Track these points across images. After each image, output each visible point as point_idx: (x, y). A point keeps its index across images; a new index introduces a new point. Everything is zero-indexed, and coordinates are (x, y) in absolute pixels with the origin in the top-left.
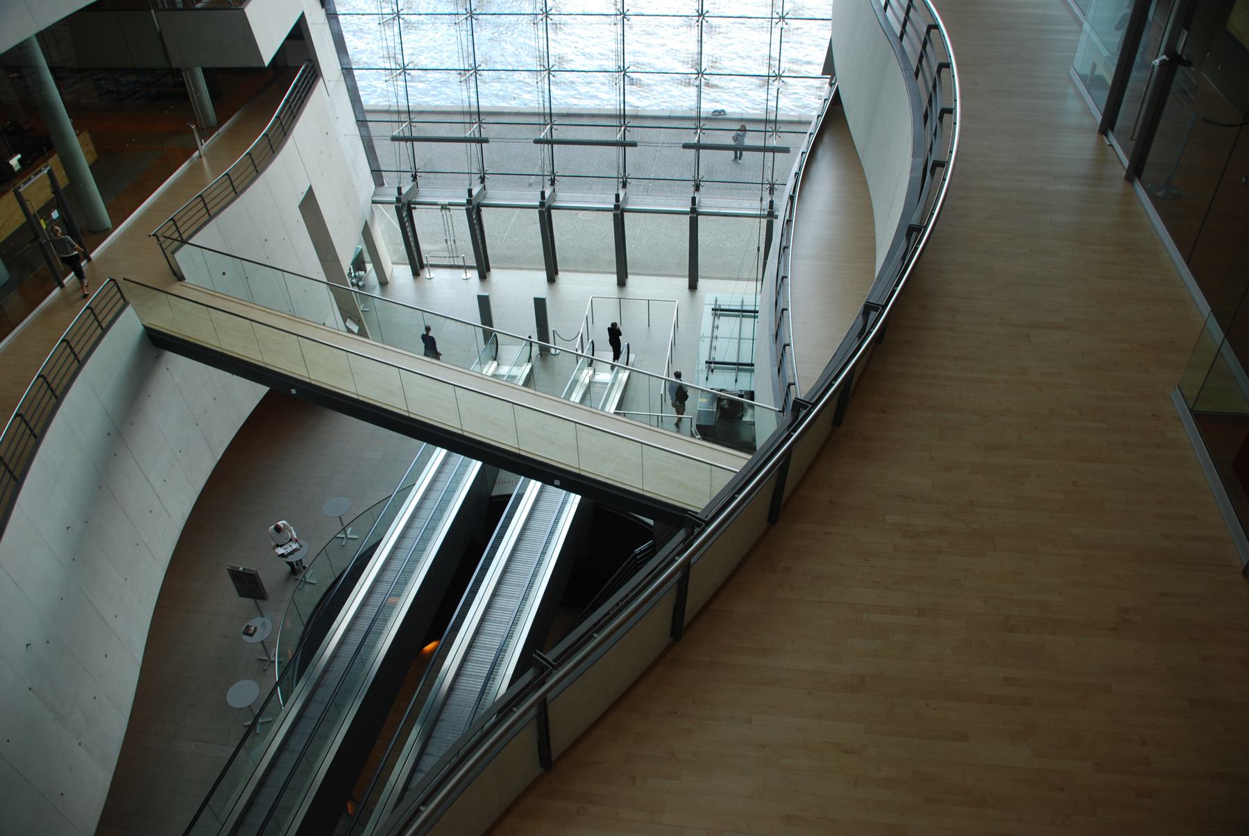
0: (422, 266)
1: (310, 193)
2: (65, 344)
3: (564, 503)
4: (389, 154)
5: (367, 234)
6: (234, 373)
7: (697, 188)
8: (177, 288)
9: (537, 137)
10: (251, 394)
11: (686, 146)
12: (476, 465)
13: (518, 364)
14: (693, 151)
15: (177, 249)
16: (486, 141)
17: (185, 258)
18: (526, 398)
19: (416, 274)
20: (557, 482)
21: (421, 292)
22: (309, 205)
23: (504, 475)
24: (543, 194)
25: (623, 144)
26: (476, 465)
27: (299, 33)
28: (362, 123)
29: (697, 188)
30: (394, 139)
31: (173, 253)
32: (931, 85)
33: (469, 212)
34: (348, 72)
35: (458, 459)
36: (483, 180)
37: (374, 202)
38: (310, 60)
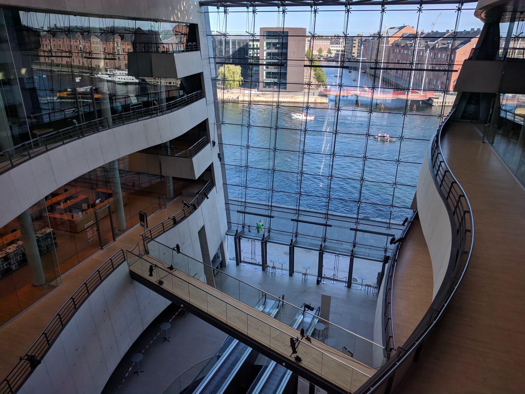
0: (241, 262)
1: (203, 228)
2: (98, 272)
3: (285, 373)
4: (236, 217)
5: (221, 247)
6: (159, 294)
7: (354, 246)
8: (145, 257)
9: (292, 218)
10: (165, 303)
11: (351, 229)
12: (249, 350)
13: (272, 308)
14: (354, 232)
15: (149, 242)
16: (273, 217)
17: (151, 246)
18: (276, 324)
19: (238, 264)
20: (284, 364)
21: (239, 270)
22: (202, 233)
23: (260, 355)
24: (292, 240)
25: (326, 225)
26: (249, 350)
27: (210, 170)
28: (227, 204)
29: (354, 246)
30: (238, 212)
31: (147, 243)
32: (460, 220)
33: (262, 243)
34: (225, 184)
35: (242, 345)
36: (269, 232)
37: (226, 234)
38: (212, 179)
